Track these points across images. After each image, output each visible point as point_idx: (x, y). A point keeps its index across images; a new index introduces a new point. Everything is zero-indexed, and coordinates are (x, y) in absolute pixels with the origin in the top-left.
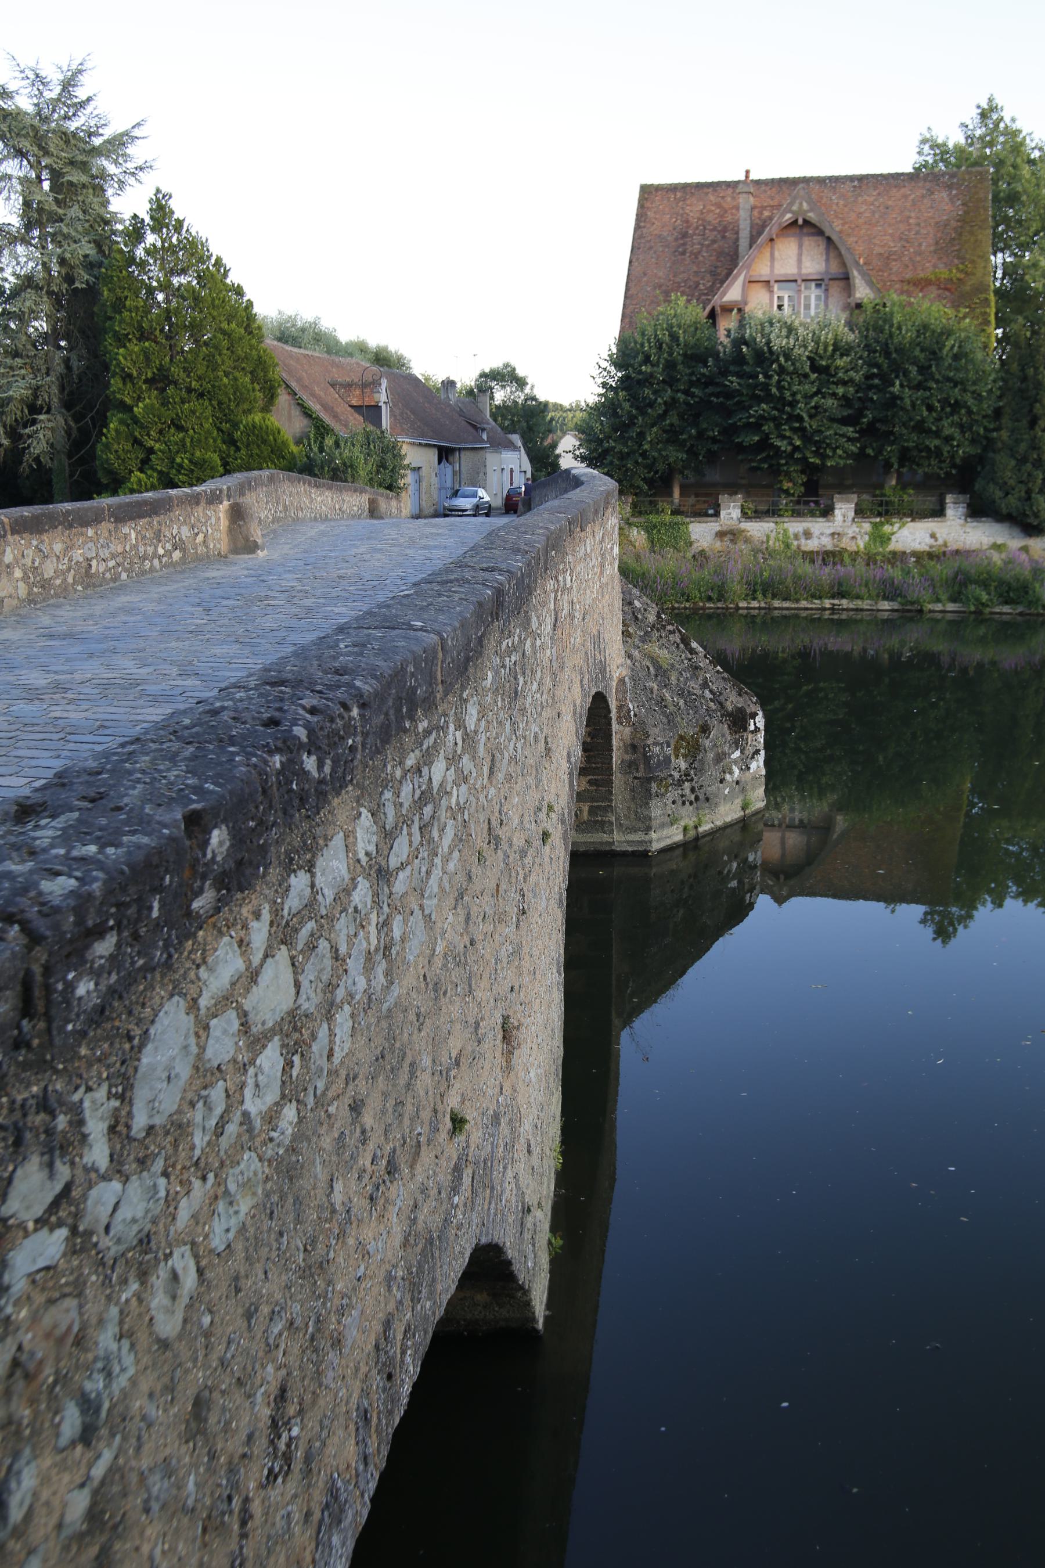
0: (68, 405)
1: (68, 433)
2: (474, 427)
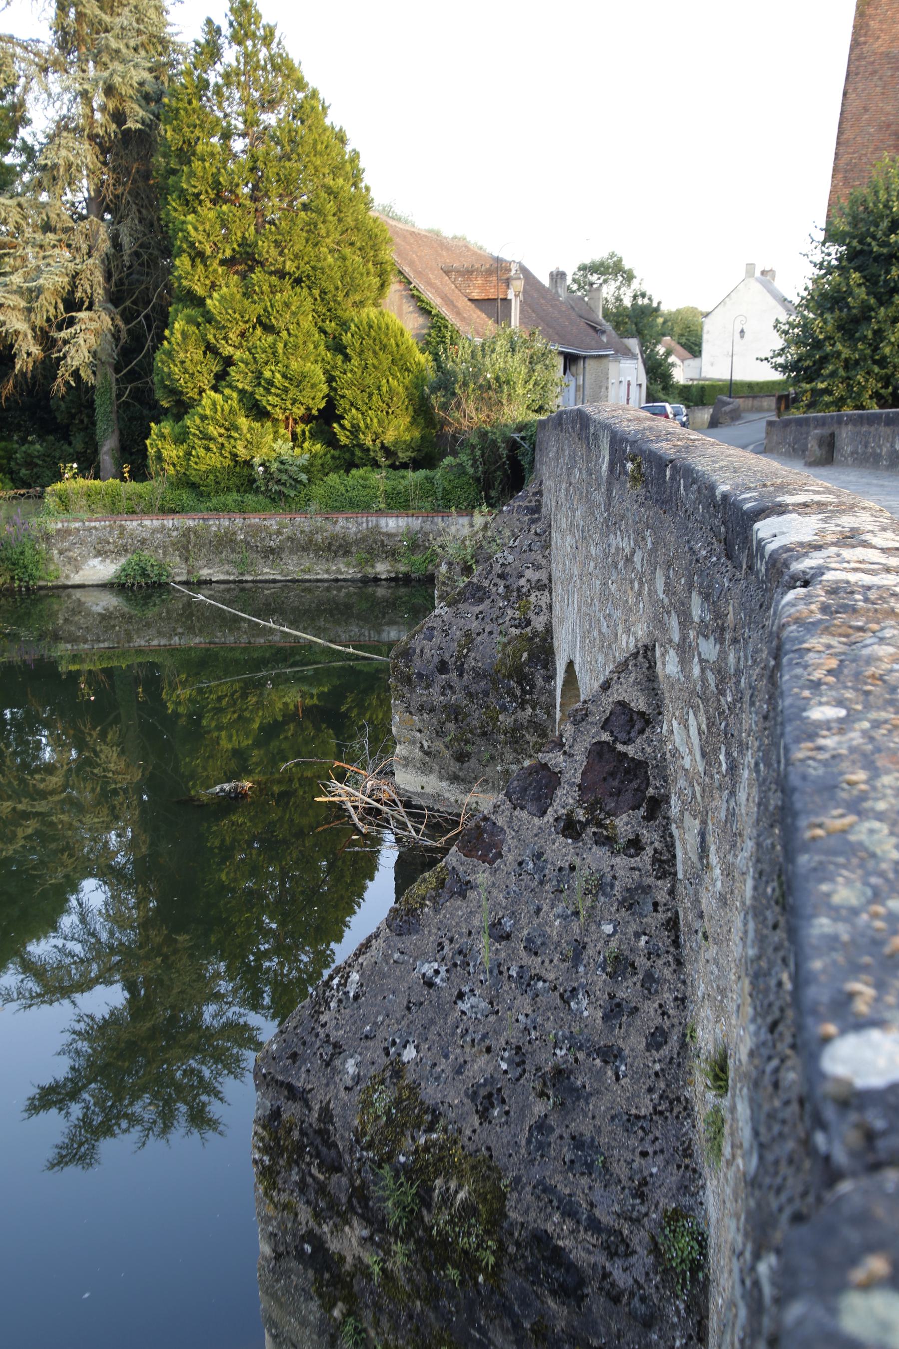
0: (115, 298)
1: (116, 337)
2: (594, 328)
